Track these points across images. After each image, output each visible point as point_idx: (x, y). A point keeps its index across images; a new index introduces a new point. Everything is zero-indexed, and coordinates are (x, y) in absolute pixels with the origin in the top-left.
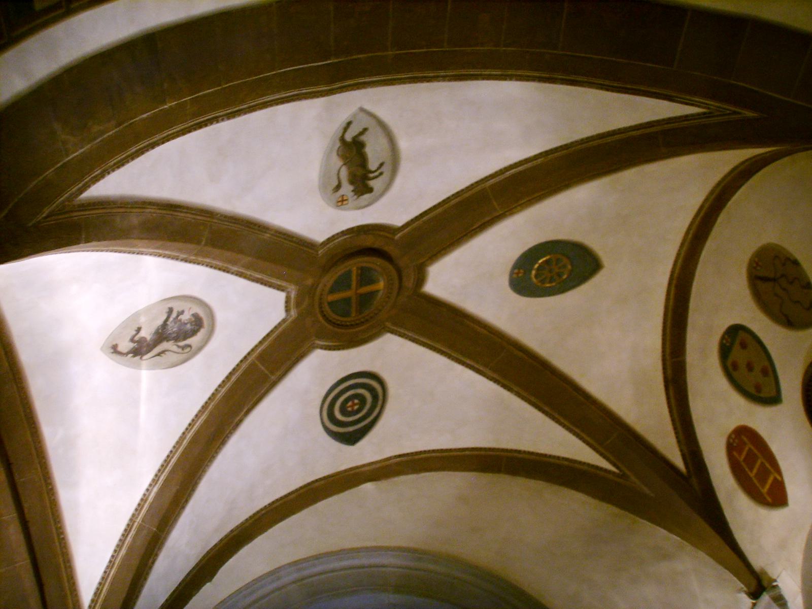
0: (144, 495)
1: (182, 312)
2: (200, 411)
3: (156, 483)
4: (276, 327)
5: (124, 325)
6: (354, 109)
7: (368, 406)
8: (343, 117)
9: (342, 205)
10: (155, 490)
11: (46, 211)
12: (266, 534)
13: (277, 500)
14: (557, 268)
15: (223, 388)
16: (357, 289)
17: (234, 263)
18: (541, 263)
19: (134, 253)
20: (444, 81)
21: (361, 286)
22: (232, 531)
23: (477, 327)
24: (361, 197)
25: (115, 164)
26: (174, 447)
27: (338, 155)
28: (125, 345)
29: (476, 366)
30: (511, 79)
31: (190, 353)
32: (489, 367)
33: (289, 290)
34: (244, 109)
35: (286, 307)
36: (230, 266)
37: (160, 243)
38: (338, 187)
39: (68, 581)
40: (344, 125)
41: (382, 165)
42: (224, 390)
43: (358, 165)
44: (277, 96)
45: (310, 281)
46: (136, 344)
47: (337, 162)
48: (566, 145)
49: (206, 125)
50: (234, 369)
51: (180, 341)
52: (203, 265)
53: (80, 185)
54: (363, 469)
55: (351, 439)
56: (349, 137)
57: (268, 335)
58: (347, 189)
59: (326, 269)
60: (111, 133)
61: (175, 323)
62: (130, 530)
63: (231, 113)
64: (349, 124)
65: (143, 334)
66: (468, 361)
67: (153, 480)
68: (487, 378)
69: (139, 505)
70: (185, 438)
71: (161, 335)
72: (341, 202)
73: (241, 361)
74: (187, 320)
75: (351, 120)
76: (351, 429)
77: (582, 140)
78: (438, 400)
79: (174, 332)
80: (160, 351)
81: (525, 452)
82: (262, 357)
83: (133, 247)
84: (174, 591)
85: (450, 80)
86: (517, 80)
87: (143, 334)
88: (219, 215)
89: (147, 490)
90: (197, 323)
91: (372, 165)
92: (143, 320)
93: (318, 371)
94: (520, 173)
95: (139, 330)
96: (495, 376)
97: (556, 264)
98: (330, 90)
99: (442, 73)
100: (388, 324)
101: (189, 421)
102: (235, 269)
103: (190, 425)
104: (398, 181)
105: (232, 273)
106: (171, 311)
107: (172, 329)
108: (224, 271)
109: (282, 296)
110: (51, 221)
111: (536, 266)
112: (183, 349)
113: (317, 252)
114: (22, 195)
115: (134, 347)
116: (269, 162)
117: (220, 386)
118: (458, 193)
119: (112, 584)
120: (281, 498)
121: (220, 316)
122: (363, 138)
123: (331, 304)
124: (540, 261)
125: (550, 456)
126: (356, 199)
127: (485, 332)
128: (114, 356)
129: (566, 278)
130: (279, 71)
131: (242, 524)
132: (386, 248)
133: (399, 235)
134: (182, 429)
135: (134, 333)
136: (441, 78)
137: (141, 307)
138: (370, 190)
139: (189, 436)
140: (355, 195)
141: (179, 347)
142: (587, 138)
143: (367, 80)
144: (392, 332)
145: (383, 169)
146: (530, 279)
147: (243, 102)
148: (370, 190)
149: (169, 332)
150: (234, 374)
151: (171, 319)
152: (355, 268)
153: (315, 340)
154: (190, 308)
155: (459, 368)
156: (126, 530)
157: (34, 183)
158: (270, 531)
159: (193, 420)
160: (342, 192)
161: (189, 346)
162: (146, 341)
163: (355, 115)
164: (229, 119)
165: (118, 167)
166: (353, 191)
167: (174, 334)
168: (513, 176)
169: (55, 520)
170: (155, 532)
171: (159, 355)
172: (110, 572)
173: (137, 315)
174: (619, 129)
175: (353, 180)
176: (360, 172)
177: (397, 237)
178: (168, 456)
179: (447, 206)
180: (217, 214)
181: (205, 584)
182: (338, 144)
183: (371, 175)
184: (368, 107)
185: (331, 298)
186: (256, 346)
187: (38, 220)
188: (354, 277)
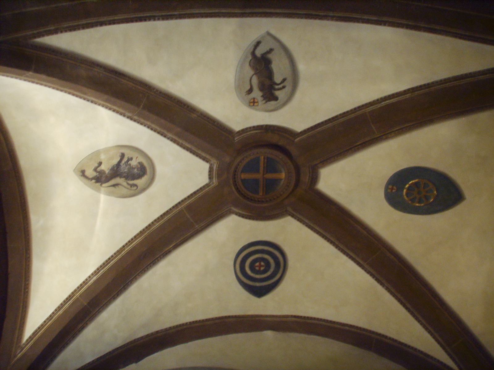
0: (86, 280)
1: (132, 159)
2: (138, 234)
3: (96, 274)
4: (201, 189)
5: (91, 157)
6: (263, 32)
7: (272, 270)
8: (254, 35)
9: (254, 105)
10: (95, 278)
12: (186, 344)
13: (196, 322)
14: (424, 191)
15: (158, 222)
16: (264, 175)
17: (169, 130)
18: (411, 184)
19: (88, 101)
20: (332, 20)
21: (267, 172)
22: (157, 332)
23: (359, 228)
24: (269, 103)
25: (67, 27)
26: (115, 254)
27: (250, 65)
28: (90, 173)
29: (358, 259)
30: (385, 25)
31: (136, 191)
32: (367, 263)
33: (212, 162)
35: (209, 175)
36: (166, 132)
37: (106, 97)
38: (250, 91)
39: (21, 320)
40: (254, 43)
41: (284, 80)
42: (157, 225)
43: (266, 77)
44: (202, 11)
45: (227, 159)
46: (98, 174)
47: (249, 72)
48: (428, 84)
49: (145, 20)
50: (167, 211)
51: (129, 180)
52: (145, 126)
53: (35, 32)
54: (266, 319)
55: (259, 292)
56: (258, 53)
57: (195, 193)
58: (257, 94)
59: (239, 152)
61: (126, 166)
62: (70, 300)
64: (258, 43)
65: (103, 167)
66: (351, 254)
67: (95, 272)
68: (365, 271)
69: (81, 285)
70: (124, 250)
71: (116, 172)
72: (253, 103)
73: (173, 207)
74: (134, 166)
76: (258, 284)
77: (441, 81)
78: (324, 281)
79: (125, 172)
80: (115, 183)
81: (390, 338)
82: (189, 208)
83: (85, 94)
84: (101, 357)
85: (337, 20)
86: (389, 26)
87: (103, 167)
88: (155, 90)
89: (90, 277)
90: (142, 171)
91: (277, 79)
92: (103, 157)
93: (231, 233)
94: (393, 104)
95: (100, 164)
96: (372, 271)
97: (424, 188)
99: (331, 14)
100: (290, 209)
101: (129, 238)
102: (169, 135)
103: (129, 242)
104: (298, 95)
105: (168, 139)
106: (123, 156)
107: (124, 170)
108: (162, 135)
109: (207, 166)
111: (407, 186)
112: (131, 187)
113: (234, 138)
115: (96, 176)
116: (200, 62)
117: (155, 220)
118: (344, 113)
119: (46, 330)
120: (200, 321)
121: (160, 169)
122: (270, 56)
123: (243, 181)
124: (410, 183)
125: (409, 346)
126: (264, 103)
127: (365, 233)
128: (82, 178)
129: (433, 201)
131: (166, 330)
132: (288, 147)
133: (298, 139)
134: (124, 243)
135: (96, 165)
137: (102, 147)
138: (276, 99)
139: (127, 249)
140: (263, 100)
141: (128, 184)
142: (445, 80)
143: (272, 11)
144: (293, 216)
145: (285, 84)
146: (402, 195)
148: (276, 99)
149: (121, 171)
150: (167, 215)
151: (123, 162)
152: (263, 157)
153: (231, 206)
154: (137, 157)
155: (344, 258)
156: (67, 299)
158: (190, 344)
159: (132, 239)
160: (253, 95)
161: (135, 185)
162: (105, 174)
163: (263, 37)
164: (163, 19)
165: (70, 30)
166: (262, 96)
167: (124, 174)
168: (388, 106)
169: (25, 278)
170: (86, 305)
171: (114, 186)
172: (48, 323)
173: (97, 153)
174: (470, 73)
175: (262, 87)
176: (267, 82)
177: (297, 140)
178: (109, 259)
179: (335, 123)
180: (154, 89)
181: (132, 363)
182: (250, 58)
183: (277, 87)
184: (273, 32)
185: (243, 176)
186: (185, 199)
188: (262, 164)
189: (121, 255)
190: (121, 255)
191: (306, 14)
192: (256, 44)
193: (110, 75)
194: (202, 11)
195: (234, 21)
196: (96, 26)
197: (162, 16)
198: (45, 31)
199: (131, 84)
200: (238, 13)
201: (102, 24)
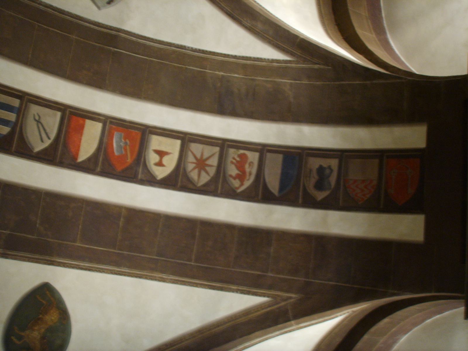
11: (316, 67)
25: (263, 62)
34: (174, 47)
44: (152, 44)
60: (260, 78)
63: (182, 49)
75: (107, 5)
98: (119, 32)
99: (41, 7)
110: (316, 61)
114: (327, 83)
130: (148, 58)
136: (43, 4)
143: (92, 26)
147: (174, 52)
157: (318, 83)
184: (94, 8)
187: (324, 66)
189: (224, 286)
190: (224, 286)
191: (63, 14)
192: (111, 3)
193: (238, 17)
194: (152, 44)
195: (127, 27)
196: (240, 57)
197: (185, 49)
198: (282, 63)
199: (223, 5)
200: (123, 33)
201: (235, 57)
